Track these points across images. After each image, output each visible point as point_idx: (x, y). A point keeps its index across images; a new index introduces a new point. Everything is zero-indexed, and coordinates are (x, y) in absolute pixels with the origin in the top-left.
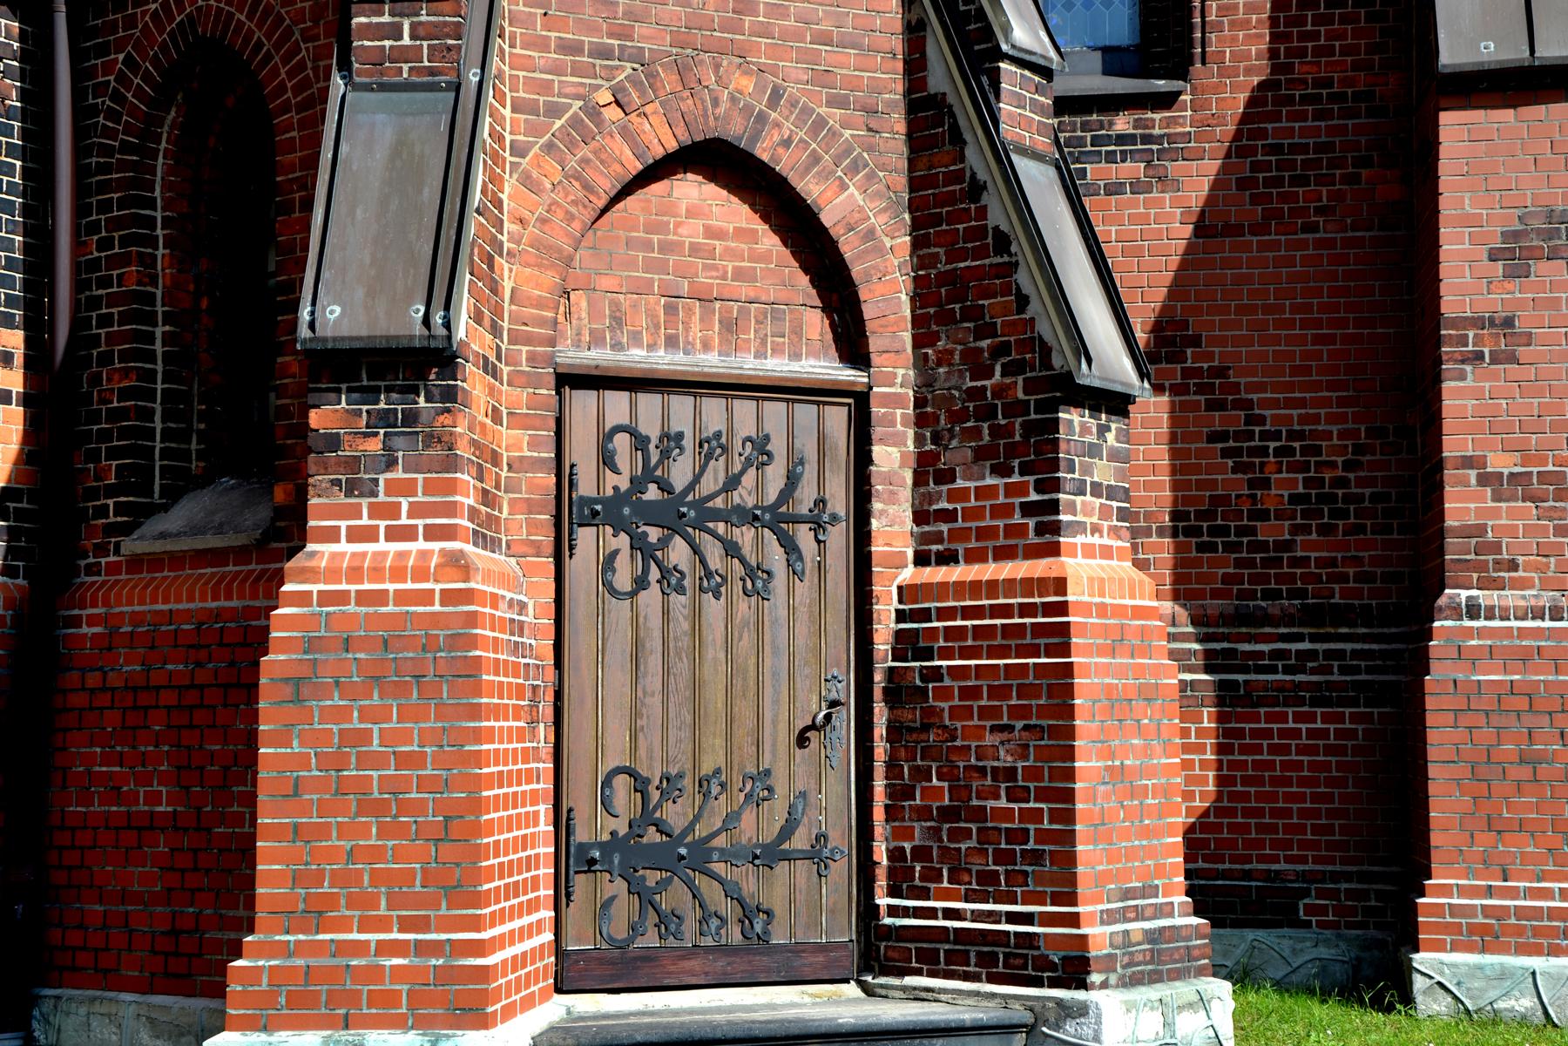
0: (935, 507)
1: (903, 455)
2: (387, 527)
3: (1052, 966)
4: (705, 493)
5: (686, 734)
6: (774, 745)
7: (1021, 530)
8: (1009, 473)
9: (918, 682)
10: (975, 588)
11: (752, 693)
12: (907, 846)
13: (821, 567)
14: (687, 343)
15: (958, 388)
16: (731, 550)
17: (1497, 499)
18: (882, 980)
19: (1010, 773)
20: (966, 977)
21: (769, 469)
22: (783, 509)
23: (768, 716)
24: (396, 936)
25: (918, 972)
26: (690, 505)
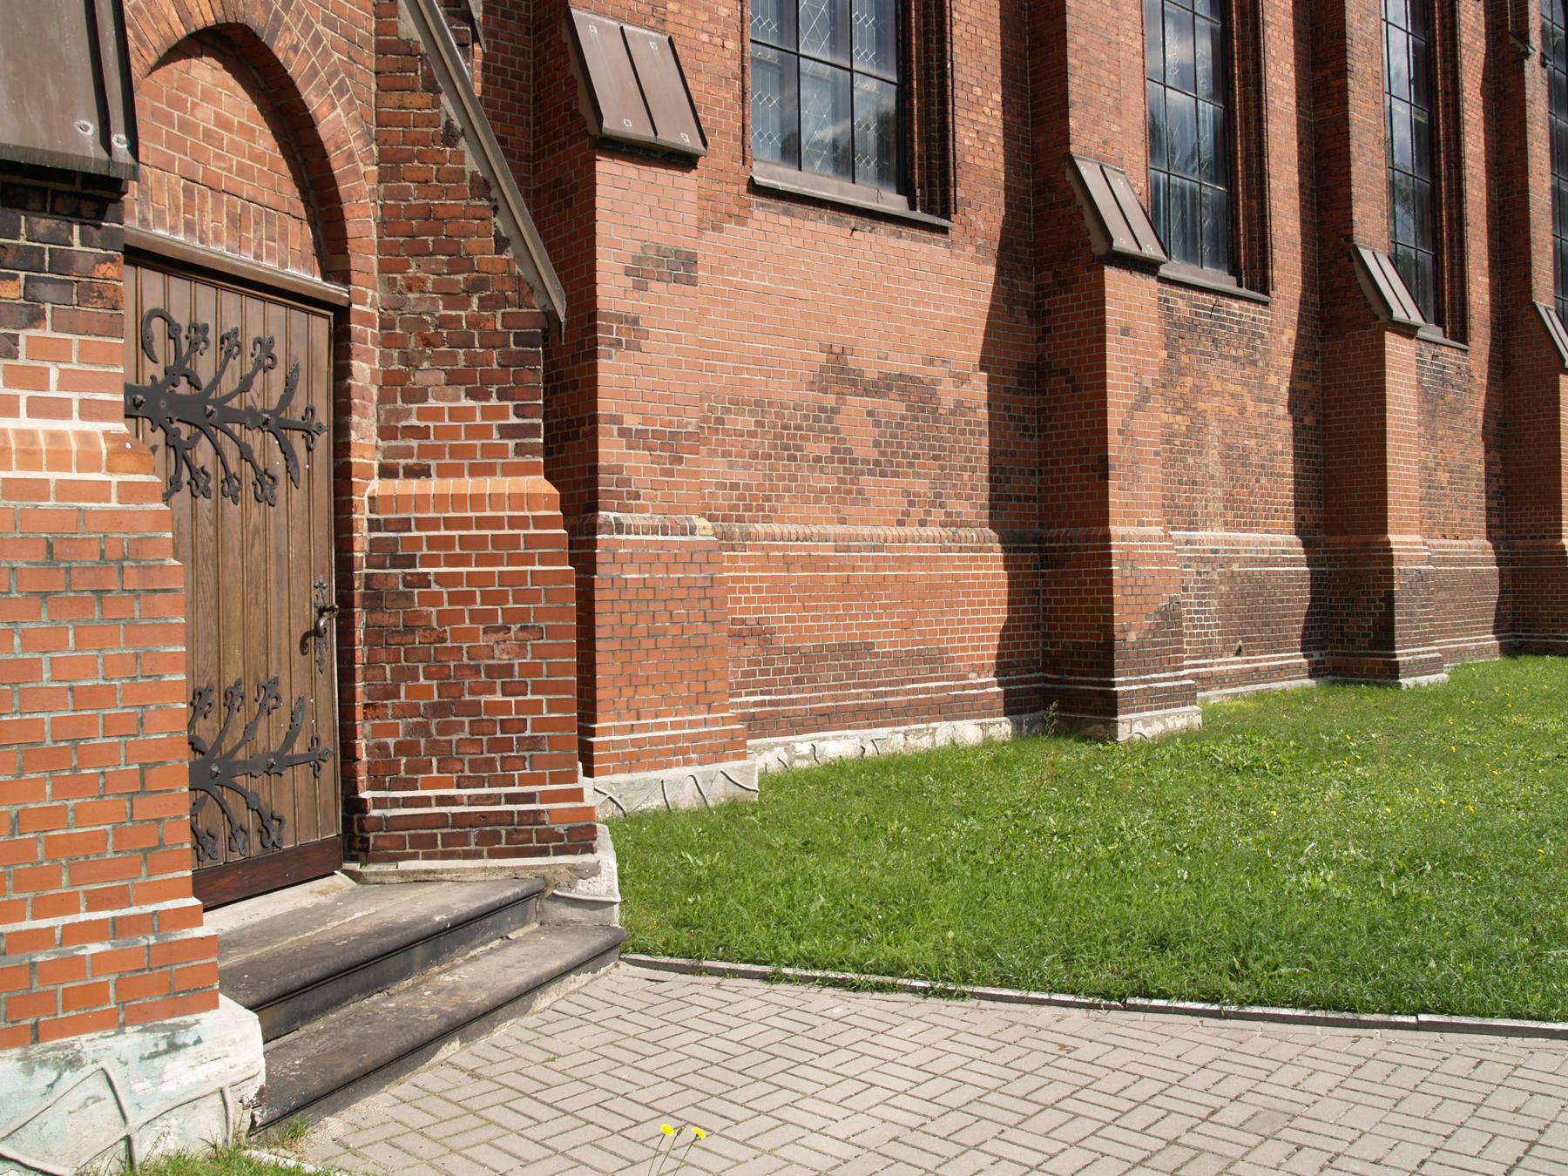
0: (403, 423)
1: (373, 372)
2: (29, 399)
3: (559, 837)
4: (225, 392)
5: (212, 646)
6: (279, 653)
7: (500, 451)
8: (487, 397)
9: (401, 588)
10: (458, 500)
11: (262, 600)
12: (391, 741)
13: (310, 473)
14: (202, 231)
15: (431, 314)
16: (245, 454)
17: (629, 447)
18: (373, 868)
19: (507, 670)
20: (467, 855)
21: (273, 373)
22: (283, 415)
23: (274, 622)
24: (84, 916)
25: (414, 857)
26: (213, 402)
